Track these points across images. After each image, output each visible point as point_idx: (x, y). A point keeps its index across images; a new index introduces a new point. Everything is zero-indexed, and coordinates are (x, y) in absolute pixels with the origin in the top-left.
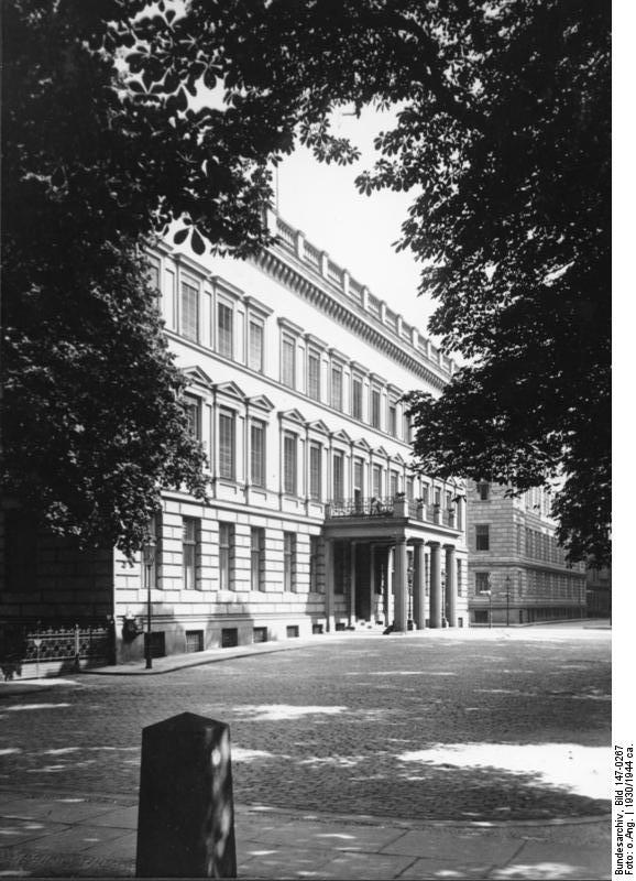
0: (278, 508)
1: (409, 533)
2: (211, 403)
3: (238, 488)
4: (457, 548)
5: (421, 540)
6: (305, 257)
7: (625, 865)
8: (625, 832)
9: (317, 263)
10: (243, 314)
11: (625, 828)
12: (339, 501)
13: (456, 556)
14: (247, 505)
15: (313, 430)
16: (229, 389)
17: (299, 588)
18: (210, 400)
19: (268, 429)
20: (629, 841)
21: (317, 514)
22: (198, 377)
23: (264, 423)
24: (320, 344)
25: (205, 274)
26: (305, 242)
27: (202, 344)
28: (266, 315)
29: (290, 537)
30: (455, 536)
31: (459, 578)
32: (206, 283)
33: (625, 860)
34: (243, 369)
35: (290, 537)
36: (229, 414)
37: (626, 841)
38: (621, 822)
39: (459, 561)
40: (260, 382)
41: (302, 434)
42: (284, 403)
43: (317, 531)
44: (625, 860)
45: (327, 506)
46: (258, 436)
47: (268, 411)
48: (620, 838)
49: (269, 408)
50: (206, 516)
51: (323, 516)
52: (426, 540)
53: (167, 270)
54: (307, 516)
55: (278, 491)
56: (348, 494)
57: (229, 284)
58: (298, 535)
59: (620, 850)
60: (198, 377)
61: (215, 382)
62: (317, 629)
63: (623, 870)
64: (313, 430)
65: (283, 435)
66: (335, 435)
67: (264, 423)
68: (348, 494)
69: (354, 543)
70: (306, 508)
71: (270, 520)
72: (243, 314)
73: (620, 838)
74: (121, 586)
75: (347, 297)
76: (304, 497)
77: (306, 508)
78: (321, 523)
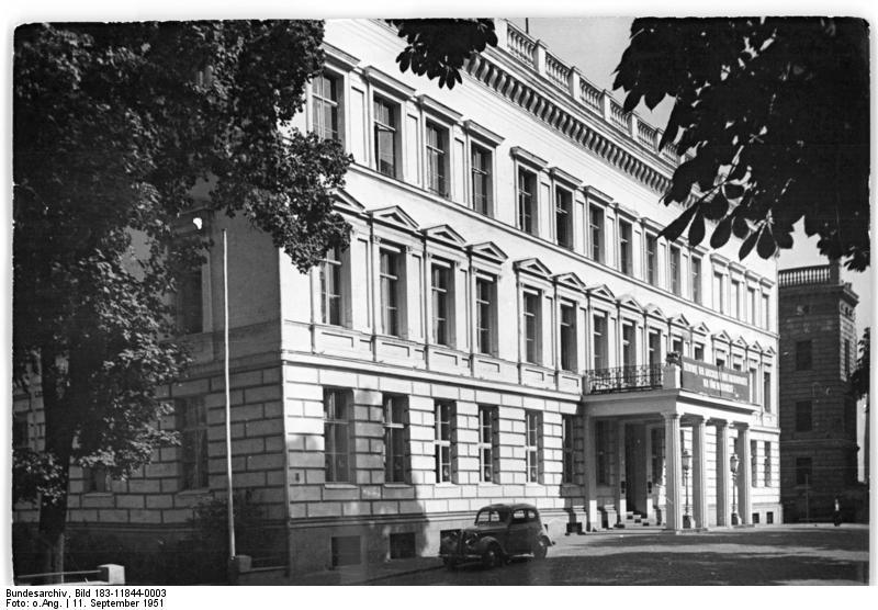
0: (517, 382)
1: (682, 409)
2: (616, 317)
3: (460, 357)
4: (751, 427)
5: (700, 419)
6: (612, 119)
7: (16, 599)
8: (49, 599)
9: (626, 125)
10: (416, 119)
11: (53, 599)
12: (601, 371)
13: (750, 436)
14: (557, 391)
15: (594, 296)
16: (534, 267)
17: (548, 479)
18: (614, 313)
19: (500, 285)
20: (40, 603)
21: (571, 387)
22: (538, 269)
23: (703, 345)
24: (343, 59)
25: (608, 201)
26: (582, 81)
27: (406, 180)
28: (494, 145)
29: (534, 418)
30: (749, 412)
31: (754, 472)
32: (577, 192)
33: (21, 599)
34: (710, 313)
35: (534, 418)
36: (571, 305)
37: (40, 600)
38: (59, 595)
39: (753, 443)
40: (465, 217)
41: (549, 291)
42: (716, 326)
43: (572, 409)
44: (21, 599)
45: (584, 379)
46: (487, 289)
47: (500, 263)
48: (43, 594)
49: (500, 258)
50: (416, 392)
51: (580, 390)
52: (707, 418)
53: (457, 139)
54: (762, 426)
55: (516, 360)
56: (614, 360)
57: (600, 193)
58: (459, 404)
59: (31, 594)
60: (538, 269)
61: (368, 208)
62: (575, 528)
63: (11, 597)
64: (594, 296)
65: (522, 290)
66: (674, 321)
67: (703, 345)
68: (614, 360)
69: (623, 423)
70: (471, 366)
71: (505, 396)
72: (416, 119)
73: (43, 594)
74: (379, 472)
75: (610, 126)
76: (468, 351)
77: (471, 366)
78: (578, 399)
